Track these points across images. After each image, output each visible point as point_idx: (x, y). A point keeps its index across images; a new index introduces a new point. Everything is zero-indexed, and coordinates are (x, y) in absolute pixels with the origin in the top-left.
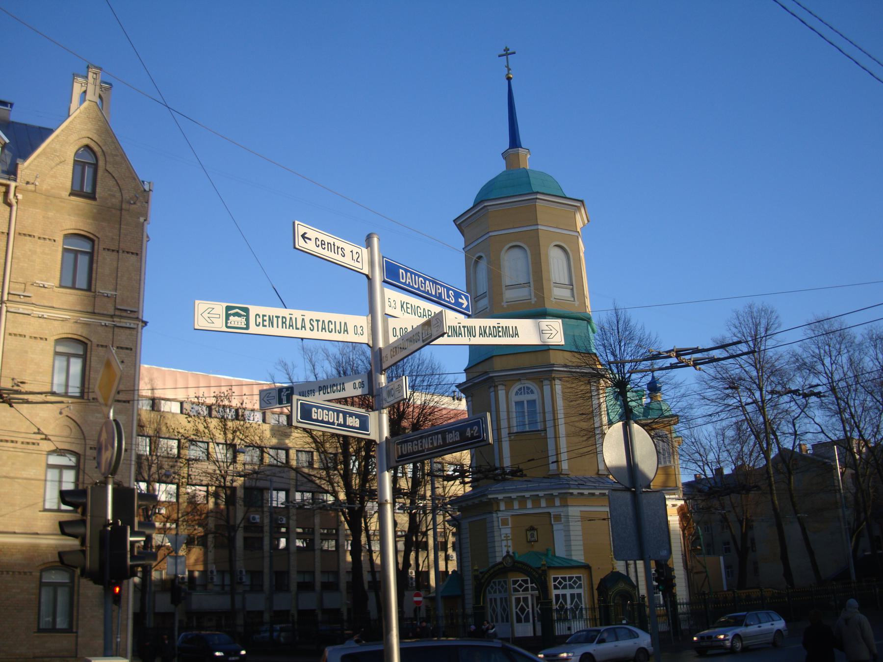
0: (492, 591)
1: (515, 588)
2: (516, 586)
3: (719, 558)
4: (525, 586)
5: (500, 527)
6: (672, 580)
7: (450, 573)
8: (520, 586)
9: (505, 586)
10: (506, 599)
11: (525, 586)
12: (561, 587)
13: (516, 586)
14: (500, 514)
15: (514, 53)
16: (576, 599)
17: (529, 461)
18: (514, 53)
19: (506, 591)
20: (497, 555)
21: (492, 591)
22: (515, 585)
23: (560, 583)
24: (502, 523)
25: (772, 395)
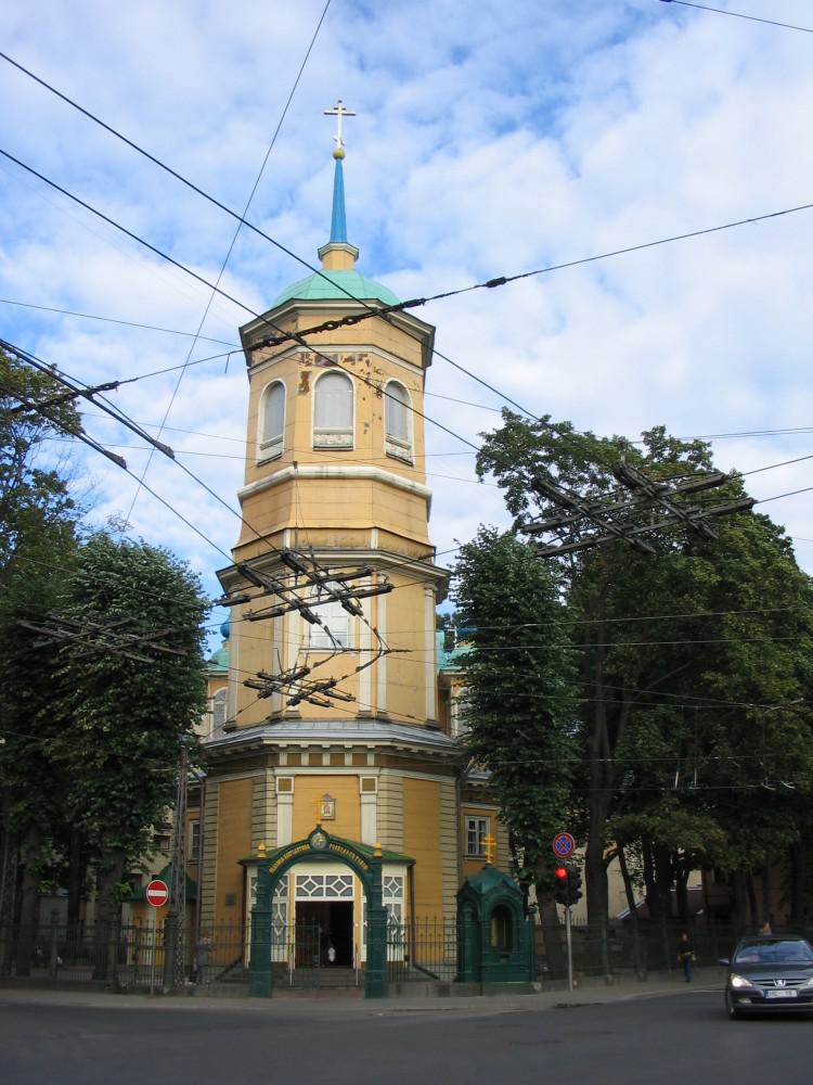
4: (318, 886)
14: (278, 771)
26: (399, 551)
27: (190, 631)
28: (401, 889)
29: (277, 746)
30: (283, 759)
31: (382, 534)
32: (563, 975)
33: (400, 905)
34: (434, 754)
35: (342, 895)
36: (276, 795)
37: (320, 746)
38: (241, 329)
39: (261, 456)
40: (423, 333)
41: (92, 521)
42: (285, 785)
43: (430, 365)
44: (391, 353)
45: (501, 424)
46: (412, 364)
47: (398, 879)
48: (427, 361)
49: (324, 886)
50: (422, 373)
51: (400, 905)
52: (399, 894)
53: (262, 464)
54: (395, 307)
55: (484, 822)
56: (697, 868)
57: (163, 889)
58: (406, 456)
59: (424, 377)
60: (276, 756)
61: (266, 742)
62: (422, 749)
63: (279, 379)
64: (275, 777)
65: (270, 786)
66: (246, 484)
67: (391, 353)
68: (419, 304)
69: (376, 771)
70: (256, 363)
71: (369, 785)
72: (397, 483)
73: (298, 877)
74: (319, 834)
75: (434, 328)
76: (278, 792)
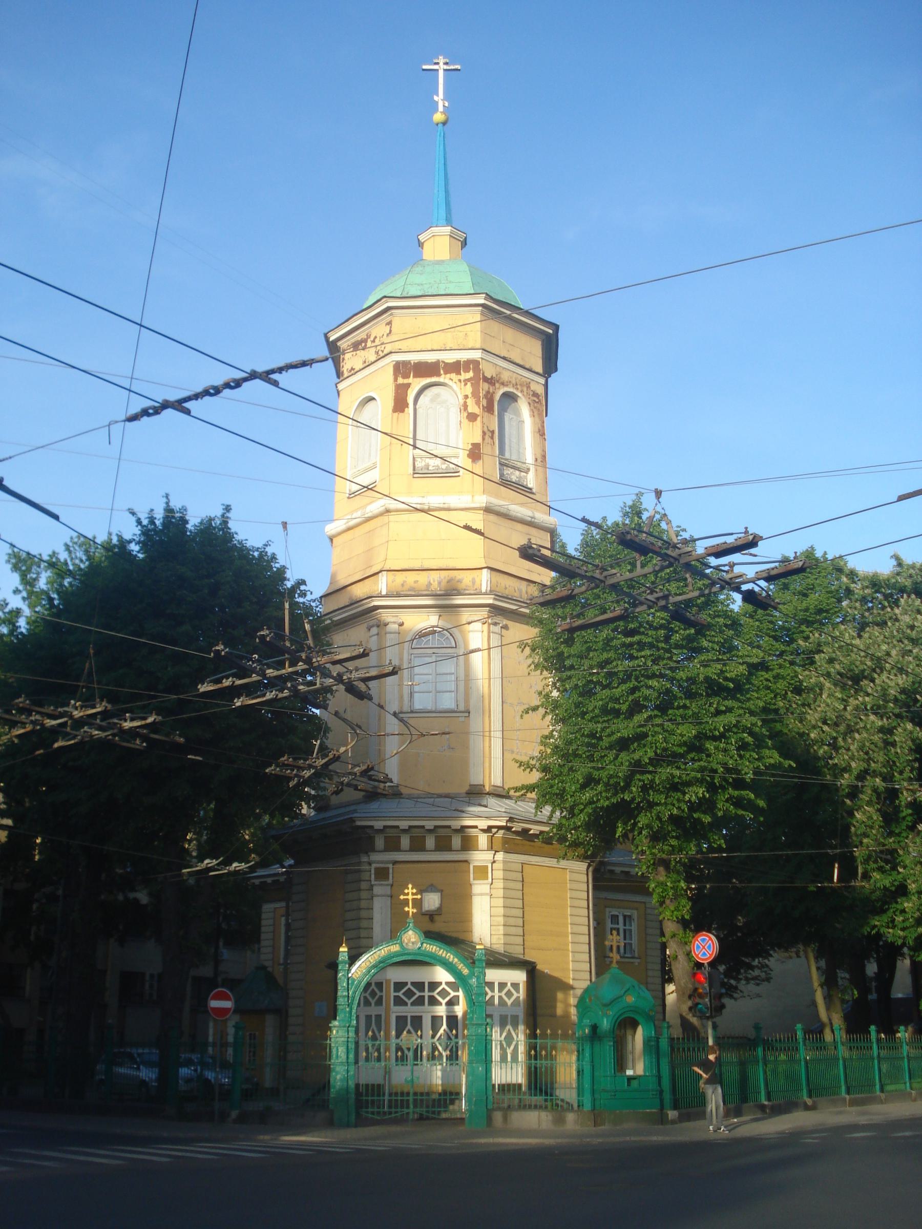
0: (373, 1002)
1: (420, 991)
2: (400, 994)
3: (214, 1009)
4: (418, 994)
5: (373, 883)
6: (826, 980)
7: (838, 971)
8: (409, 994)
9: (379, 994)
10: (378, 1017)
11: (418, 994)
12: (409, 986)
13: (400, 994)
14: (374, 857)
15: (228, 508)
17: (901, 498)
18: (228, 508)
19: (379, 1002)
20: (501, 900)
21: (373, 1002)
22: (399, 991)
23: (409, 994)
24: (375, 874)
25: (840, 748)
26: (516, 595)
29: (372, 827)
30: (380, 842)
31: (494, 573)
33: (517, 1016)
34: (274, 881)
36: (372, 886)
37: (423, 827)
41: (239, 537)
42: (382, 874)
43: (556, 370)
44: (504, 358)
46: (530, 370)
47: (515, 986)
48: (550, 364)
49: (426, 994)
50: (542, 381)
51: (517, 1016)
54: (255, 378)
55: (630, 917)
56: (178, 1070)
59: (546, 386)
60: (371, 840)
61: (359, 823)
62: (262, 880)
64: (370, 864)
65: (365, 876)
67: (504, 358)
68: (307, 365)
70: (345, 376)
72: (513, 513)
73: (395, 984)
75: (556, 328)
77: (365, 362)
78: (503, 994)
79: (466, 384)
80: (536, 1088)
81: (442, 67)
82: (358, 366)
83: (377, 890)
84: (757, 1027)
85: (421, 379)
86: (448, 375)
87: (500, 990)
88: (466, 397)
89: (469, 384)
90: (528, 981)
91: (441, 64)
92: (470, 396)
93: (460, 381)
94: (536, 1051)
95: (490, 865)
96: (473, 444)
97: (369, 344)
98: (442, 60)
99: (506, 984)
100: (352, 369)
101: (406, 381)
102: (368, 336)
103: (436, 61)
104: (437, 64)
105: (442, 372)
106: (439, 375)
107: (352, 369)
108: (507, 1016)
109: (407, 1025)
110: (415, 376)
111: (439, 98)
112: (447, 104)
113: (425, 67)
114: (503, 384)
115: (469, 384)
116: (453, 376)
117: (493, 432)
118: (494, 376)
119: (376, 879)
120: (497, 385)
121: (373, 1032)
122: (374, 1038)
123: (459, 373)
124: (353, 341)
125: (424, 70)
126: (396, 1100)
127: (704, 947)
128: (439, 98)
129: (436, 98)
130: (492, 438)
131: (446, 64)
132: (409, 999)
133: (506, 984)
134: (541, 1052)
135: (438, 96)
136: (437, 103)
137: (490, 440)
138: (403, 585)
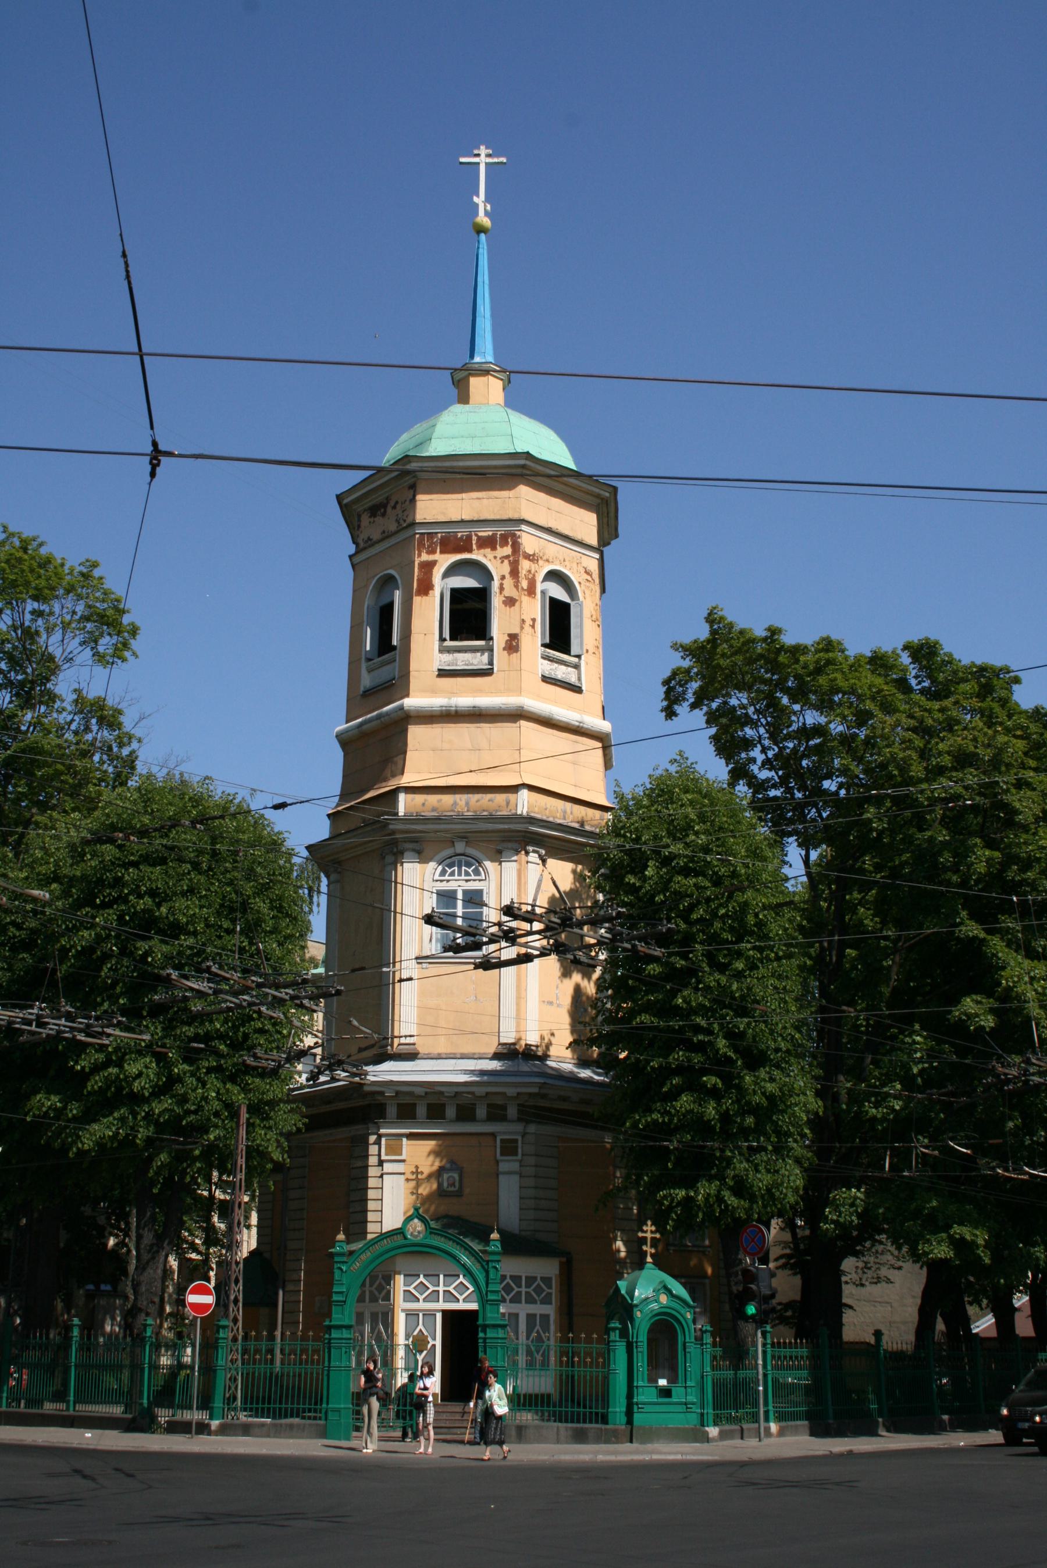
16: (421, 1327)
27: (999, 754)
28: (458, 1300)
32: (197, 1423)
33: (547, 1316)
35: (464, 1300)
38: (339, 498)
39: (366, 681)
40: (598, 496)
45: (703, 632)
47: (547, 1280)
49: (523, 1290)
52: (546, 1301)
53: (367, 694)
57: (193, 1305)
58: (573, 679)
63: (392, 572)
66: (347, 722)
69: (519, 1127)
71: (509, 1148)
74: (416, 1221)
76: (383, 1157)
77: (384, 532)
78: (373, 1289)
79: (502, 562)
80: (573, 1401)
81: (483, 160)
82: (376, 536)
83: (503, 1167)
84: (878, 1334)
85: (449, 556)
86: (482, 551)
87: (528, 1286)
88: (503, 578)
89: (506, 562)
90: (561, 1274)
91: (483, 155)
92: (507, 576)
93: (495, 557)
94: (307, 1356)
95: (520, 1138)
96: (510, 635)
97: (389, 509)
98: (483, 151)
99: (535, 1278)
100: (369, 539)
101: (431, 558)
102: (388, 499)
103: (476, 152)
104: (478, 155)
105: (474, 547)
106: (470, 551)
107: (369, 539)
108: (535, 1315)
109: (535, 1325)
110: (442, 552)
111: (480, 200)
112: (489, 207)
113: (463, 160)
114: (548, 561)
115: (506, 562)
116: (488, 551)
117: (534, 620)
118: (537, 551)
119: (502, 1154)
120: (541, 562)
121: (538, 1332)
122: (539, 1339)
123: (494, 548)
124: (370, 504)
125: (461, 163)
126: (573, 1412)
127: (753, 1241)
128: (480, 200)
129: (475, 199)
130: (533, 626)
131: (488, 156)
132: (534, 1290)
133: (377, 1276)
134: (573, 1357)
135: (478, 196)
136: (477, 205)
137: (530, 630)
138: (423, 804)
